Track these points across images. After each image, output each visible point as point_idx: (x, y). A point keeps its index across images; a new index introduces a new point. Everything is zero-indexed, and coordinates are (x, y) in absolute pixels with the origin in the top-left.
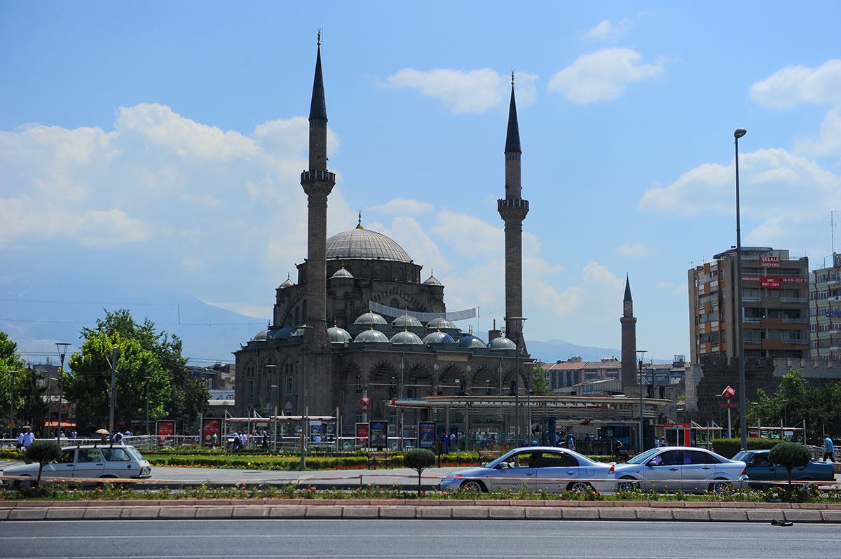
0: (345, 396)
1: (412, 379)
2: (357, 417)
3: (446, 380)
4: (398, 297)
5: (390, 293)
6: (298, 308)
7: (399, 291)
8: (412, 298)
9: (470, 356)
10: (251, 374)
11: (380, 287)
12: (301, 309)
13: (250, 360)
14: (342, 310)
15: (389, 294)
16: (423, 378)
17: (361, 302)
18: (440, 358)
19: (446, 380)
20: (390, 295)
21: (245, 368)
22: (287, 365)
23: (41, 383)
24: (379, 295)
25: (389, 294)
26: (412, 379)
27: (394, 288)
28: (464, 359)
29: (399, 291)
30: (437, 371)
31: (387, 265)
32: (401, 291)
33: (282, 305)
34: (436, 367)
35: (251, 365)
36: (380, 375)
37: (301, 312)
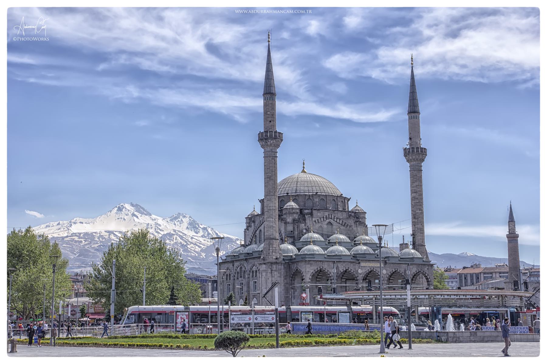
0: (294, 293)
4: (332, 221)
5: (326, 218)
8: (343, 221)
11: (319, 214)
15: (325, 219)
17: (305, 225)
18: (363, 264)
20: (326, 219)
24: (318, 220)
25: (325, 219)
27: (329, 215)
32: (334, 216)
34: (360, 271)
37: (263, 233)
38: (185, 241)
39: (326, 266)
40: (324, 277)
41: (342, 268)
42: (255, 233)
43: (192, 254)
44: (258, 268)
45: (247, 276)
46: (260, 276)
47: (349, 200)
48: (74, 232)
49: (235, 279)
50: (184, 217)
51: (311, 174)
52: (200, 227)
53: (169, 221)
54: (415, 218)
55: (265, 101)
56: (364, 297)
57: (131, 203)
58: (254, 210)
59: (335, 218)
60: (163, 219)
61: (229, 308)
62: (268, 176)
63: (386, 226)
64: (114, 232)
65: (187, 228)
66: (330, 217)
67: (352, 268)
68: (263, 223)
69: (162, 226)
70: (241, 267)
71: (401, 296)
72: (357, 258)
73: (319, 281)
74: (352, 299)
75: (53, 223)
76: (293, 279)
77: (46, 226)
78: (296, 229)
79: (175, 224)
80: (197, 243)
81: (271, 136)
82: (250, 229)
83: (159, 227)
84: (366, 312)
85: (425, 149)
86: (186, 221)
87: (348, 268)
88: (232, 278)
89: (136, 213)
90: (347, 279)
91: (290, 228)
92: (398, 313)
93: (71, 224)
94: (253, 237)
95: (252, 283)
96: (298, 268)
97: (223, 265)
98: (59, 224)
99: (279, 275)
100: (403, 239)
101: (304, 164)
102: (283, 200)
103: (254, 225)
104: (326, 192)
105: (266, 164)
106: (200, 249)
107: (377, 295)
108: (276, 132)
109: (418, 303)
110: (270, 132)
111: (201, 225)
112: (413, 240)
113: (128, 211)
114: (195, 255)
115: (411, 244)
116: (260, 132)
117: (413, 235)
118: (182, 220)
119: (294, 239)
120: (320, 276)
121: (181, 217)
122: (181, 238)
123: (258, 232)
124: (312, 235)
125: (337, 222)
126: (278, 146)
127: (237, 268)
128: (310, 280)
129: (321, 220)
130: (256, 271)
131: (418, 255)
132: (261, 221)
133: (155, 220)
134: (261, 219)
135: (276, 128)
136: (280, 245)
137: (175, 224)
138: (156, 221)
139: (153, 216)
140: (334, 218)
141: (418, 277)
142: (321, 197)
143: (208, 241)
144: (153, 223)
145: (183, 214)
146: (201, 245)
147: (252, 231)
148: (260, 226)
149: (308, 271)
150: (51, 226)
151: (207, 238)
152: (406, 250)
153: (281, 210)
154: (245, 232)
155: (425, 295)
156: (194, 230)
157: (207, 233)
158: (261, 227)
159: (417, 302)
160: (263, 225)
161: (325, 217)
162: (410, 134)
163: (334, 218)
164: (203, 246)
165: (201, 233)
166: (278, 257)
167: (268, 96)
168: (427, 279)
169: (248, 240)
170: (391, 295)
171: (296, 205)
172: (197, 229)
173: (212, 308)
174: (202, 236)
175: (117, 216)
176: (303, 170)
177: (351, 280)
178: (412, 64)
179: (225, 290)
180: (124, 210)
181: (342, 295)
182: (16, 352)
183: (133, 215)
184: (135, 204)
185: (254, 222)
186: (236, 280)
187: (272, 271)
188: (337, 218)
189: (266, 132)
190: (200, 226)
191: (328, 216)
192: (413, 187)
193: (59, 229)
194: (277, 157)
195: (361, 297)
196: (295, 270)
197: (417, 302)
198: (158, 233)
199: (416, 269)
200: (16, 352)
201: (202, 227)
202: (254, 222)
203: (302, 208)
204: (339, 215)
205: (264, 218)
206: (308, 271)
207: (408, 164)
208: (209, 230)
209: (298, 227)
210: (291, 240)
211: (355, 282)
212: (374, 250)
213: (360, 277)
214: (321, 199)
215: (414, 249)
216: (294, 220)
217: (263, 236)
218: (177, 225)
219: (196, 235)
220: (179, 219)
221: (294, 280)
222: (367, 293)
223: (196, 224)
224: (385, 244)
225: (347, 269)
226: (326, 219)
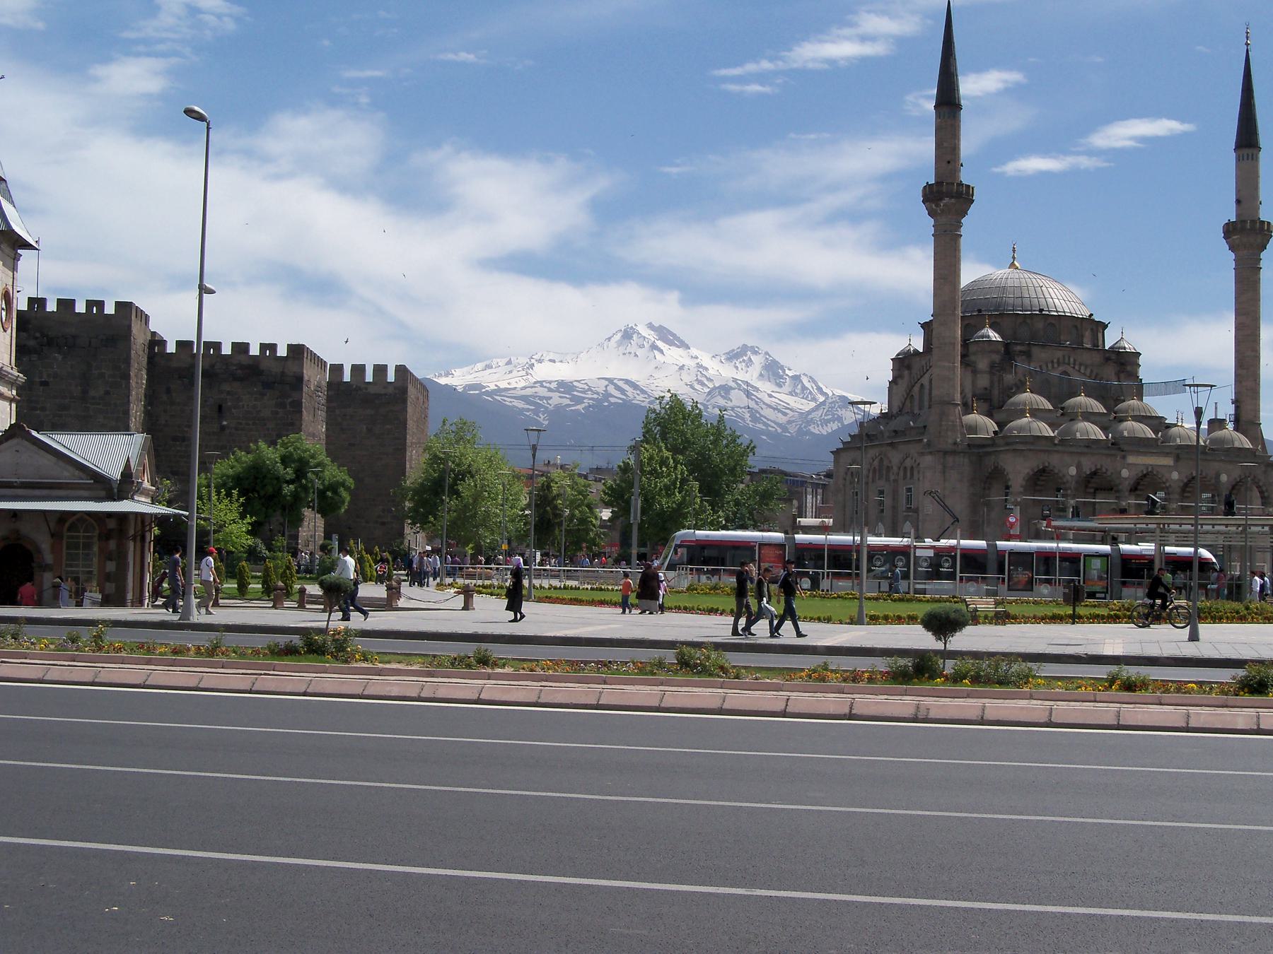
4: (1070, 370)
5: (1058, 363)
7: (1072, 360)
8: (1092, 371)
15: (1056, 365)
18: (1131, 459)
20: (1058, 366)
22: (905, 468)
25: (1056, 365)
27: (1064, 356)
28: (1168, 461)
29: (1072, 360)
30: (1126, 479)
31: (1053, 322)
32: (1075, 360)
36: (1042, 486)
37: (927, 391)
38: (756, 401)
39: (1054, 461)
41: (1088, 465)
42: (910, 391)
43: (770, 429)
44: (915, 461)
45: (892, 478)
46: (921, 478)
47: (1105, 326)
48: (539, 380)
50: (756, 353)
51: (1037, 274)
52: (787, 375)
53: (723, 361)
54: (1241, 366)
56: (1138, 526)
58: (910, 345)
59: (1077, 363)
60: (713, 357)
61: (959, 543)
63: (1212, 386)
65: (761, 375)
66: (1067, 361)
67: (1106, 463)
68: (927, 370)
69: (711, 371)
70: (881, 458)
71: (1263, 528)
72: (1118, 446)
74: (1111, 530)
75: (499, 360)
77: (486, 366)
78: (996, 384)
79: (737, 368)
82: (900, 381)
83: (705, 373)
84: (1147, 557)
85: (1269, 223)
86: (758, 360)
87: (1102, 466)
89: (660, 344)
90: (1096, 489)
91: (983, 381)
92: (1214, 560)
93: (533, 364)
94: (906, 399)
96: (998, 463)
98: (509, 363)
100: (1216, 408)
101: (1014, 251)
102: (971, 326)
103: (910, 374)
104: (1058, 310)
107: (1164, 524)
108: (961, 184)
109: (1230, 541)
110: (947, 183)
111: (790, 370)
112: (1236, 410)
113: (642, 339)
114: (776, 430)
115: (1232, 419)
116: (927, 183)
117: (1237, 402)
118: (750, 359)
119: (994, 403)
120: (1043, 481)
121: (749, 353)
122: (748, 395)
123: (916, 389)
124: (1027, 396)
125: (1079, 371)
126: (964, 213)
127: (874, 461)
128: (1022, 489)
129: (1047, 366)
130: (912, 467)
131: (1247, 444)
132: (923, 367)
133: (697, 358)
135: (959, 177)
136: (963, 416)
137: (737, 368)
138: (699, 360)
139: (694, 351)
140: (1074, 364)
141: (1243, 489)
144: (692, 363)
145: (752, 347)
146: (787, 411)
148: (921, 377)
149: (1018, 469)
150: (494, 367)
151: (801, 396)
152: (1219, 434)
153: (965, 343)
154: (890, 389)
155: (1263, 526)
157: (799, 387)
158: (922, 379)
159: (1230, 539)
160: (927, 376)
161: (1055, 361)
163: (1074, 364)
165: (787, 388)
166: (958, 440)
168: (1261, 492)
169: (896, 404)
170: (1227, 526)
171: (996, 335)
172: (781, 377)
173: (1063, 548)
174: (790, 394)
175: (622, 349)
176: (1013, 262)
177: (1104, 490)
178: (1247, 44)
180: (635, 336)
181: (1092, 520)
182: (474, 609)
183: (654, 347)
185: (909, 367)
187: (944, 467)
188: (1081, 365)
189: (939, 183)
190: (787, 372)
193: (511, 372)
194: (961, 236)
195: (1144, 526)
196: (993, 467)
197: (1230, 539)
198: (703, 384)
200: (474, 609)
201: (790, 373)
202: (909, 367)
203: (1009, 341)
204: (1086, 358)
205: (930, 360)
206: (1018, 469)
208: (805, 380)
209: (999, 381)
210: (985, 406)
212: (1156, 432)
214: (1049, 324)
215: (1237, 431)
216: (992, 366)
217: (926, 398)
218: (740, 369)
219: (777, 389)
220: (744, 358)
221: (989, 489)
222: (1144, 518)
223: (779, 368)
224: (1177, 418)
225: (1099, 469)
226: (1058, 366)
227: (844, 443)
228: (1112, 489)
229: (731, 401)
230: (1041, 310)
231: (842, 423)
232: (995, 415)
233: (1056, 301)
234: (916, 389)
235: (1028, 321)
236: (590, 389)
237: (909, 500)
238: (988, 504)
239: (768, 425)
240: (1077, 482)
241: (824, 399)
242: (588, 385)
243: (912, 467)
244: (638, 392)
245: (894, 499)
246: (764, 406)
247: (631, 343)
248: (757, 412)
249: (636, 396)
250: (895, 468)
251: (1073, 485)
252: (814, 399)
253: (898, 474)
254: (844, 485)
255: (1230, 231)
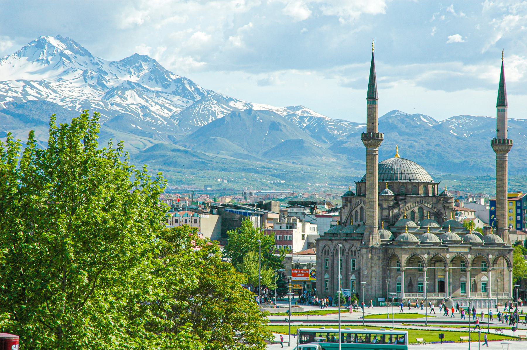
0: (390, 274)
1: (432, 262)
2: (398, 287)
3: (455, 262)
6: (356, 211)
9: (470, 248)
10: (327, 254)
12: (359, 212)
13: (326, 245)
14: (387, 216)
16: (439, 261)
18: (451, 250)
19: (455, 262)
21: (323, 250)
22: (352, 251)
23: (201, 257)
26: (432, 262)
27: (420, 200)
28: (467, 250)
31: (416, 185)
33: (346, 208)
35: (327, 248)
36: (412, 261)
37: (359, 214)
40: (416, 260)
45: (345, 254)
49: (333, 256)
52: (171, 79)
55: (368, 105)
57: (58, 36)
62: (370, 172)
64: (31, 82)
73: (411, 263)
76: (390, 262)
80: (165, 105)
81: (373, 136)
87: (438, 253)
88: (330, 254)
94: (349, 216)
95: (350, 261)
97: (322, 241)
99: (377, 258)
103: (351, 205)
105: (368, 161)
106: (170, 114)
114: (163, 123)
123: (354, 212)
130: (355, 251)
134: (357, 201)
137: (130, 72)
142: (414, 184)
143: (183, 102)
146: (172, 108)
147: (348, 210)
156: (161, 82)
157: (181, 88)
158: (357, 208)
162: (498, 125)
164: (175, 109)
167: (371, 100)
179: (323, 264)
184: (64, 37)
186: (335, 256)
189: (369, 133)
191: (419, 202)
192: (499, 176)
199: (497, 253)
201: (173, 77)
207: (495, 154)
211: (442, 264)
213: (448, 261)
219: (164, 90)
220: (137, 65)
221: (390, 263)
227: (321, 236)
228: (442, 261)
229: (127, 99)
230: (410, 180)
231: (215, 117)
232: (391, 228)
233: (417, 175)
234: (354, 212)
235: (405, 185)
236: (10, 89)
237: (354, 265)
238: (389, 270)
239: (157, 119)
240: (428, 261)
241: (200, 98)
242: (8, 86)
243: (355, 251)
244: (51, 92)
245: (346, 264)
246: (153, 104)
247: (43, 52)
248: (147, 107)
249: (49, 94)
250: (347, 251)
251: (426, 262)
252: (193, 98)
253: (348, 253)
254: (322, 256)
255: (494, 143)
